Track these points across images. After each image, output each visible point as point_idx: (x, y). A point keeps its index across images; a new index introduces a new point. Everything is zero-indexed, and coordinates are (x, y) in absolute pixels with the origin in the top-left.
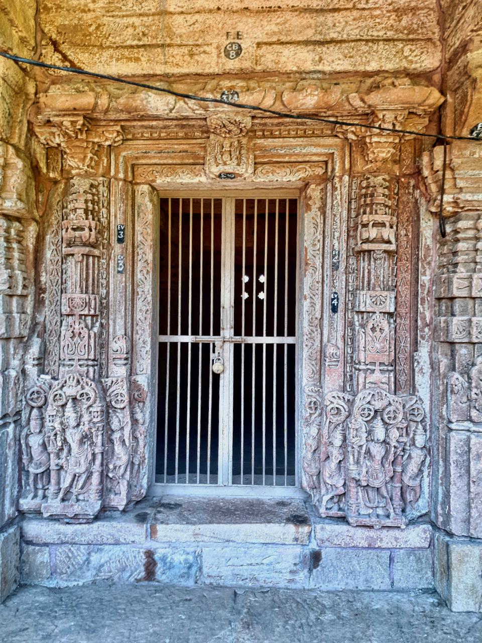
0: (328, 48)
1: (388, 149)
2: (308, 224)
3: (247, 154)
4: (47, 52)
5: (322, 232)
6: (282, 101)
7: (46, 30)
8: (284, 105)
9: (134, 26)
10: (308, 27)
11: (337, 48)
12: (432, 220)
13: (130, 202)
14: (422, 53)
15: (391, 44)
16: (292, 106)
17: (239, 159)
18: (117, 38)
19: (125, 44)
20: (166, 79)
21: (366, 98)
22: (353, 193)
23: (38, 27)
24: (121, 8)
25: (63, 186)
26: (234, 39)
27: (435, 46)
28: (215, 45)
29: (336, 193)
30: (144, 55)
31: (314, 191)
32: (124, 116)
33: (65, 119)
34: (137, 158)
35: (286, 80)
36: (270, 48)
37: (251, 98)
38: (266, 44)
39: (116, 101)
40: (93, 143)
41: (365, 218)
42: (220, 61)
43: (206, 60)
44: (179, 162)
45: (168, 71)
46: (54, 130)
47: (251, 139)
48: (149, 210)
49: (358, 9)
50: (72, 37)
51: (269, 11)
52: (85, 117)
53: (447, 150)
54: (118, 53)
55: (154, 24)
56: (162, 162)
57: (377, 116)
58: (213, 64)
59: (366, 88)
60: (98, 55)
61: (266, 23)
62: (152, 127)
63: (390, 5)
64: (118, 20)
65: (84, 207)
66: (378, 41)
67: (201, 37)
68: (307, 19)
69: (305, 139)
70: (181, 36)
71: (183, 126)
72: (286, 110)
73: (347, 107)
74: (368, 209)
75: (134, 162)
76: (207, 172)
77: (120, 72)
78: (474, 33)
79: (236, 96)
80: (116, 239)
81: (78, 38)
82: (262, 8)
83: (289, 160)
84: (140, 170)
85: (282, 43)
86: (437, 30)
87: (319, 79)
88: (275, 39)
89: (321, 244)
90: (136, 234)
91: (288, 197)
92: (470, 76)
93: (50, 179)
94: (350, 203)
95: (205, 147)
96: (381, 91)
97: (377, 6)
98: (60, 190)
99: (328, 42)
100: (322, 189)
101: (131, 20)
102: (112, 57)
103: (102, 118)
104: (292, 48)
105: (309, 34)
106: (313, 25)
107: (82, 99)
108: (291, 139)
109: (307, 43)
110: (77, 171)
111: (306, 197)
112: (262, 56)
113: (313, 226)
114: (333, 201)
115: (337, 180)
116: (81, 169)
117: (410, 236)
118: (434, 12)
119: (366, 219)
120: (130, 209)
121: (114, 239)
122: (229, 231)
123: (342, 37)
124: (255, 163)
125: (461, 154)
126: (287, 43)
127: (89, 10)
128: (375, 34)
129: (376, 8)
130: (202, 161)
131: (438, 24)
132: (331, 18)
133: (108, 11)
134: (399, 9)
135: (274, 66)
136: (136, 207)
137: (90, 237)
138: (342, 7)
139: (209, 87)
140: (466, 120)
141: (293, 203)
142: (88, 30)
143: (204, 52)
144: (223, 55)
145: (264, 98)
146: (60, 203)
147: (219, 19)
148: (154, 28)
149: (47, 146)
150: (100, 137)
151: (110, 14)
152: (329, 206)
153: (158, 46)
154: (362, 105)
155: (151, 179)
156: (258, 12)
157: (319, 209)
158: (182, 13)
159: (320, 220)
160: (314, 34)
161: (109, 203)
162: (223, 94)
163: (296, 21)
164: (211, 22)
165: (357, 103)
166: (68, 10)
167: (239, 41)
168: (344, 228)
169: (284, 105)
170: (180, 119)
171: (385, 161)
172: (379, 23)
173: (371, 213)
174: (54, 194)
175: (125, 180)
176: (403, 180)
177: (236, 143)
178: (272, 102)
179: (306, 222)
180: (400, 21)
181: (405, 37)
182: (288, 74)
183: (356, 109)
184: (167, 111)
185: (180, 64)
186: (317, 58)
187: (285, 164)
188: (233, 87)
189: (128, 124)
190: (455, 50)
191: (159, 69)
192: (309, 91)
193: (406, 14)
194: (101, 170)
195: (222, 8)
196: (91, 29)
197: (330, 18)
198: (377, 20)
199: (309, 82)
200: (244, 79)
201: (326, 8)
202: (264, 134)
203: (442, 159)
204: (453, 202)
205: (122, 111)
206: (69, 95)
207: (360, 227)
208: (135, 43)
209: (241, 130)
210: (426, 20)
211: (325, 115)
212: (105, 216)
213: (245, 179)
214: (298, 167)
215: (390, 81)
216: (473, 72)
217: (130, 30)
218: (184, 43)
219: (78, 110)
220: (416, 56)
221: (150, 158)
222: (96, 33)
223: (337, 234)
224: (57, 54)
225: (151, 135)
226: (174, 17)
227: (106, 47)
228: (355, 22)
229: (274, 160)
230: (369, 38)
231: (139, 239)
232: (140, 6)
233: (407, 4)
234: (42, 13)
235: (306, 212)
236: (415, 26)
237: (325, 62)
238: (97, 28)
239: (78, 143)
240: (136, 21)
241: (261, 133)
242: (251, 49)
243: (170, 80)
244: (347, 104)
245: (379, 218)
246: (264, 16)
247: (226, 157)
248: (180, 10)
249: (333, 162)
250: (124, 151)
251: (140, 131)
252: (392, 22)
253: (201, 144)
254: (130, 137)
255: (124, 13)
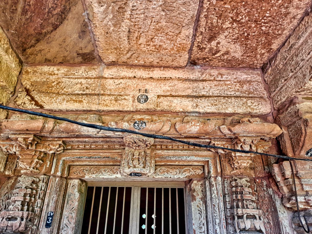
0: (201, 100)
1: (248, 161)
2: (194, 211)
3: (151, 160)
4: (21, 96)
5: (205, 217)
6: (175, 128)
7: (24, 83)
8: (176, 131)
9: (81, 84)
10: (188, 89)
11: (206, 100)
12: (286, 212)
13: (62, 193)
14: (259, 104)
15: (239, 99)
16: (182, 132)
17: (145, 163)
18: (70, 89)
19: (74, 93)
20: (99, 113)
21: (232, 129)
22: (226, 190)
23: (19, 82)
24: (75, 74)
25: (13, 181)
26: (144, 93)
27: (266, 101)
28: (132, 96)
29: (213, 189)
30: (85, 100)
31: (196, 186)
32: (64, 135)
33: (20, 136)
34: (73, 161)
35: (176, 116)
36: (165, 98)
37: (154, 126)
38: (163, 96)
39: (59, 126)
40: (41, 152)
41: (240, 211)
42: (134, 104)
43: (126, 103)
44: (102, 164)
45: (100, 108)
46: (13, 143)
47: (153, 150)
48: (76, 198)
49: (217, 80)
50: (40, 87)
51: (164, 80)
52: (35, 135)
53: (292, 164)
54: (68, 98)
55: (94, 83)
56: (90, 164)
57: (240, 140)
58: (130, 106)
59: (229, 123)
60: (55, 98)
61: (163, 86)
62: (85, 142)
63: (235, 79)
64: (72, 80)
65: (22, 200)
66: (231, 97)
67: (123, 91)
68: (187, 84)
69: (189, 151)
70: (110, 90)
71: (107, 142)
72: (178, 134)
73: (219, 133)
74: (240, 204)
75: (70, 164)
76: (122, 172)
77: (68, 108)
78: (298, 93)
79: (144, 124)
80: (45, 224)
81: (44, 88)
82: (161, 78)
83: (178, 164)
84: (73, 170)
85: (173, 96)
86: (265, 93)
87: (196, 116)
88: (168, 94)
89: (206, 227)
90: (63, 217)
91: (177, 187)
92: (301, 118)
93: (5, 176)
94: (224, 196)
95: (121, 155)
96: (242, 125)
97: (228, 79)
98: (10, 184)
99: (200, 97)
100: (202, 184)
101: (80, 81)
102: (64, 100)
103: (48, 136)
104: (179, 99)
105: (189, 92)
106: (191, 88)
107: (34, 124)
108: (180, 151)
109: (188, 96)
110: (25, 171)
111: (190, 190)
112: (161, 102)
113: (198, 212)
114: (211, 195)
115: (212, 179)
116: (28, 170)
117: (272, 224)
118: (261, 83)
119: (241, 212)
120: (61, 198)
121: (43, 224)
122: (135, 212)
123: (209, 94)
124: (156, 165)
125: (303, 169)
126: (176, 96)
127: (54, 74)
128: (229, 93)
129: (227, 81)
130: (119, 164)
131: (265, 89)
132: (202, 84)
133: (66, 75)
134: (240, 81)
135: (169, 108)
136: (67, 196)
137: (20, 226)
138: (208, 79)
139: (126, 118)
140: (303, 145)
141: (181, 191)
142: (51, 85)
143: (125, 99)
144: (136, 101)
145: (163, 126)
146: (7, 195)
147: (135, 83)
148: (94, 85)
149: (8, 153)
150: (46, 148)
151: (68, 77)
152: (208, 197)
153: (96, 95)
154: (229, 132)
155: (81, 175)
156: (158, 80)
157: (202, 199)
158: (112, 78)
159: (203, 208)
160: (192, 92)
161: (45, 195)
162: (135, 123)
163: (181, 85)
164: (130, 83)
165: (226, 131)
166: (41, 74)
167: (147, 94)
168: (223, 217)
169: (176, 131)
170: (105, 137)
171: (245, 168)
172: (230, 88)
173: (243, 207)
174: (4, 187)
175: (61, 177)
176: (258, 180)
177: (143, 152)
178: (168, 129)
179: (193, 209)
180: (242, 87)
181: (247, 96)
182: (177, 113)
183: (225, 135)
184: (96, 133)
185: (108, 105)
186: (195, 105)
187: (175, 167)
188: (143, 119)
189: (68, 140)
190: (282, 104)
191: (94, 107)
192: (193, 123)
193: (245, 84)
194: (44, 170)
195: (137, 77)
196: (53, 84)
197: (201, 85)
198: (229, 86)
199: (191, 118)
200: (149, 115)
201: (198, 79)
202: (161, 147)
203: (291, 170)
204: (304, 202)
205: (63, 132)
206: (25, 121)
207: (236, 217)
208: (80, 92)
209: (147, 145)
210: (257, 87)
211: (203, 138)
212: (39, 205)
213: (148, 176)
214: (184, 169)
215: (247, 119)
216: (303, 115)
217: (79, 86)
218: (112, 93)
219: (30, 131)
220: (255, 106)
221: (82, 161)
222: (56, 86)
223: (218, 221)
224: (27, 97)
225: (85, 147)
226: (107, 80)
227: (61, 94)
228: (216, 87)
229: (168, 164)
230: (226, 95)
231: (65, 222)
232: (87, 74)
233: (245, 79)
234: (24, 74)
235: (193, 201)
236: (252, 90)
237: (200, 107)
238: (57, 84)
239: (28, 152)
240: (83, 81)
241: (160, 147)
242: (154, 98)
243: (100, 114)
244: (219, 132)
245: (251, 212)
246: (161, 82)
247: (136, 162)
248: (111, 76)
249: (208, 167)
250: (64, 156)
251: (77, 144)
252: (238, 88)
253: (119, 152)
254: (69, 147)
255: (76, 77)
